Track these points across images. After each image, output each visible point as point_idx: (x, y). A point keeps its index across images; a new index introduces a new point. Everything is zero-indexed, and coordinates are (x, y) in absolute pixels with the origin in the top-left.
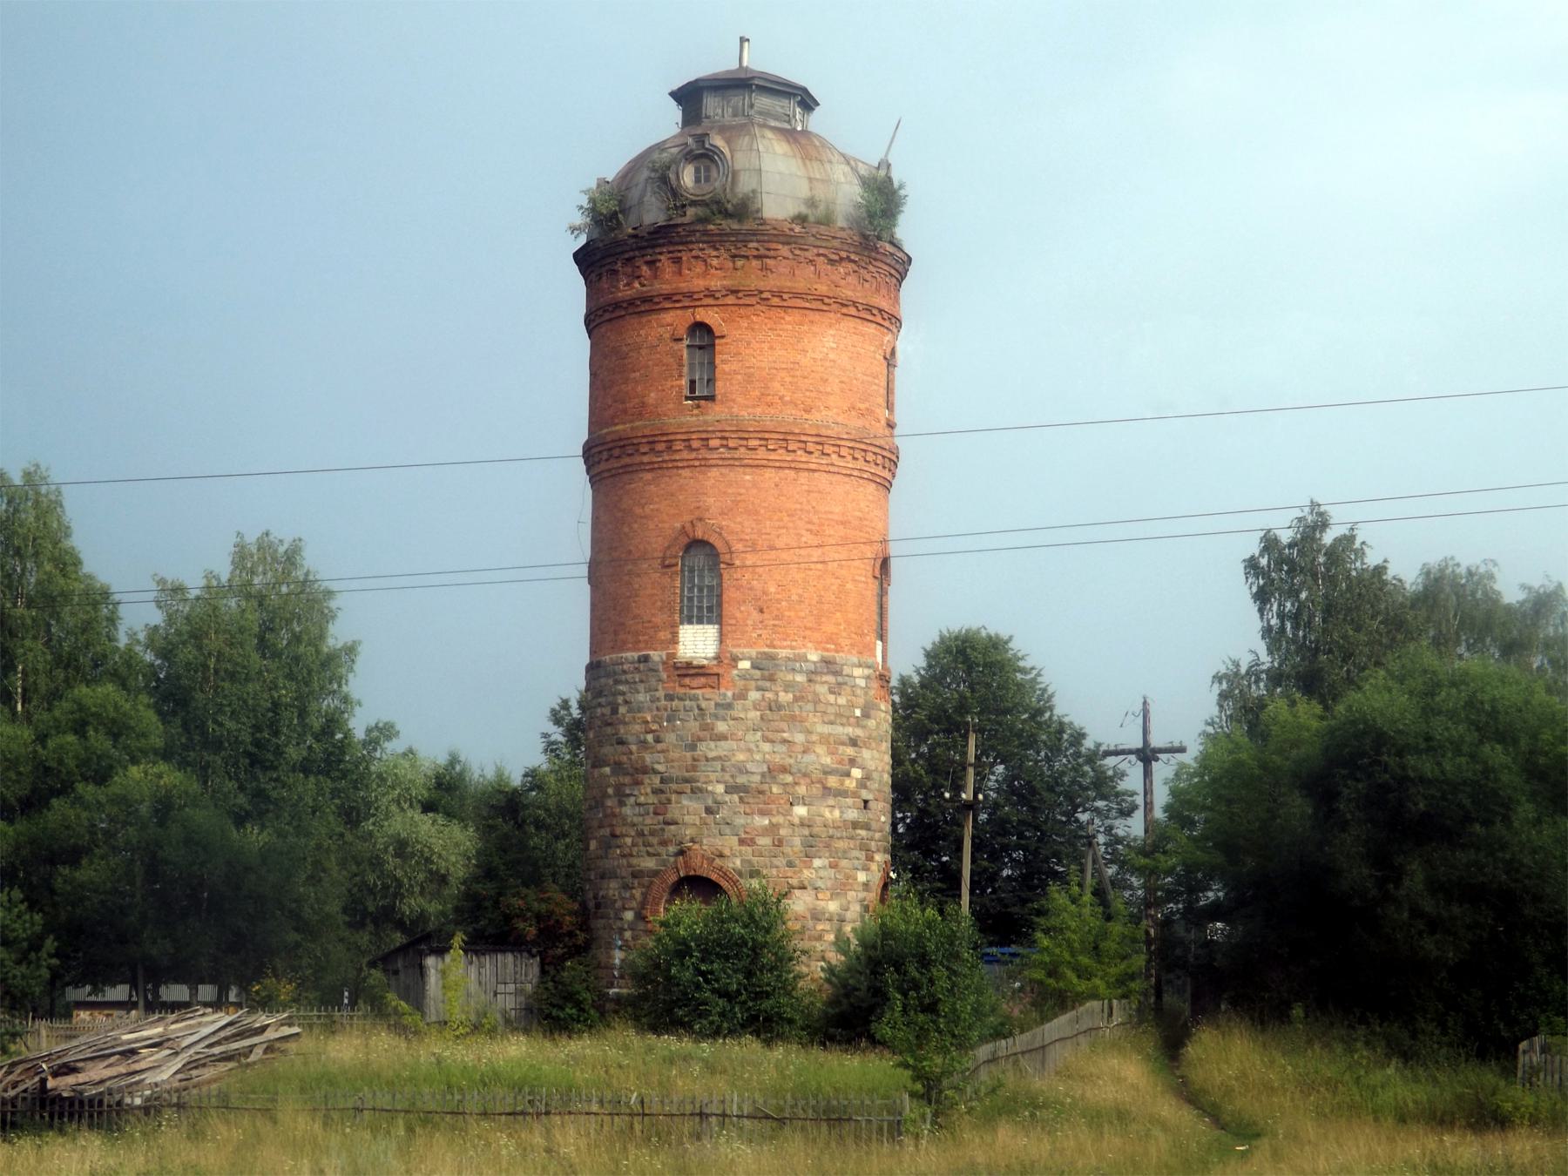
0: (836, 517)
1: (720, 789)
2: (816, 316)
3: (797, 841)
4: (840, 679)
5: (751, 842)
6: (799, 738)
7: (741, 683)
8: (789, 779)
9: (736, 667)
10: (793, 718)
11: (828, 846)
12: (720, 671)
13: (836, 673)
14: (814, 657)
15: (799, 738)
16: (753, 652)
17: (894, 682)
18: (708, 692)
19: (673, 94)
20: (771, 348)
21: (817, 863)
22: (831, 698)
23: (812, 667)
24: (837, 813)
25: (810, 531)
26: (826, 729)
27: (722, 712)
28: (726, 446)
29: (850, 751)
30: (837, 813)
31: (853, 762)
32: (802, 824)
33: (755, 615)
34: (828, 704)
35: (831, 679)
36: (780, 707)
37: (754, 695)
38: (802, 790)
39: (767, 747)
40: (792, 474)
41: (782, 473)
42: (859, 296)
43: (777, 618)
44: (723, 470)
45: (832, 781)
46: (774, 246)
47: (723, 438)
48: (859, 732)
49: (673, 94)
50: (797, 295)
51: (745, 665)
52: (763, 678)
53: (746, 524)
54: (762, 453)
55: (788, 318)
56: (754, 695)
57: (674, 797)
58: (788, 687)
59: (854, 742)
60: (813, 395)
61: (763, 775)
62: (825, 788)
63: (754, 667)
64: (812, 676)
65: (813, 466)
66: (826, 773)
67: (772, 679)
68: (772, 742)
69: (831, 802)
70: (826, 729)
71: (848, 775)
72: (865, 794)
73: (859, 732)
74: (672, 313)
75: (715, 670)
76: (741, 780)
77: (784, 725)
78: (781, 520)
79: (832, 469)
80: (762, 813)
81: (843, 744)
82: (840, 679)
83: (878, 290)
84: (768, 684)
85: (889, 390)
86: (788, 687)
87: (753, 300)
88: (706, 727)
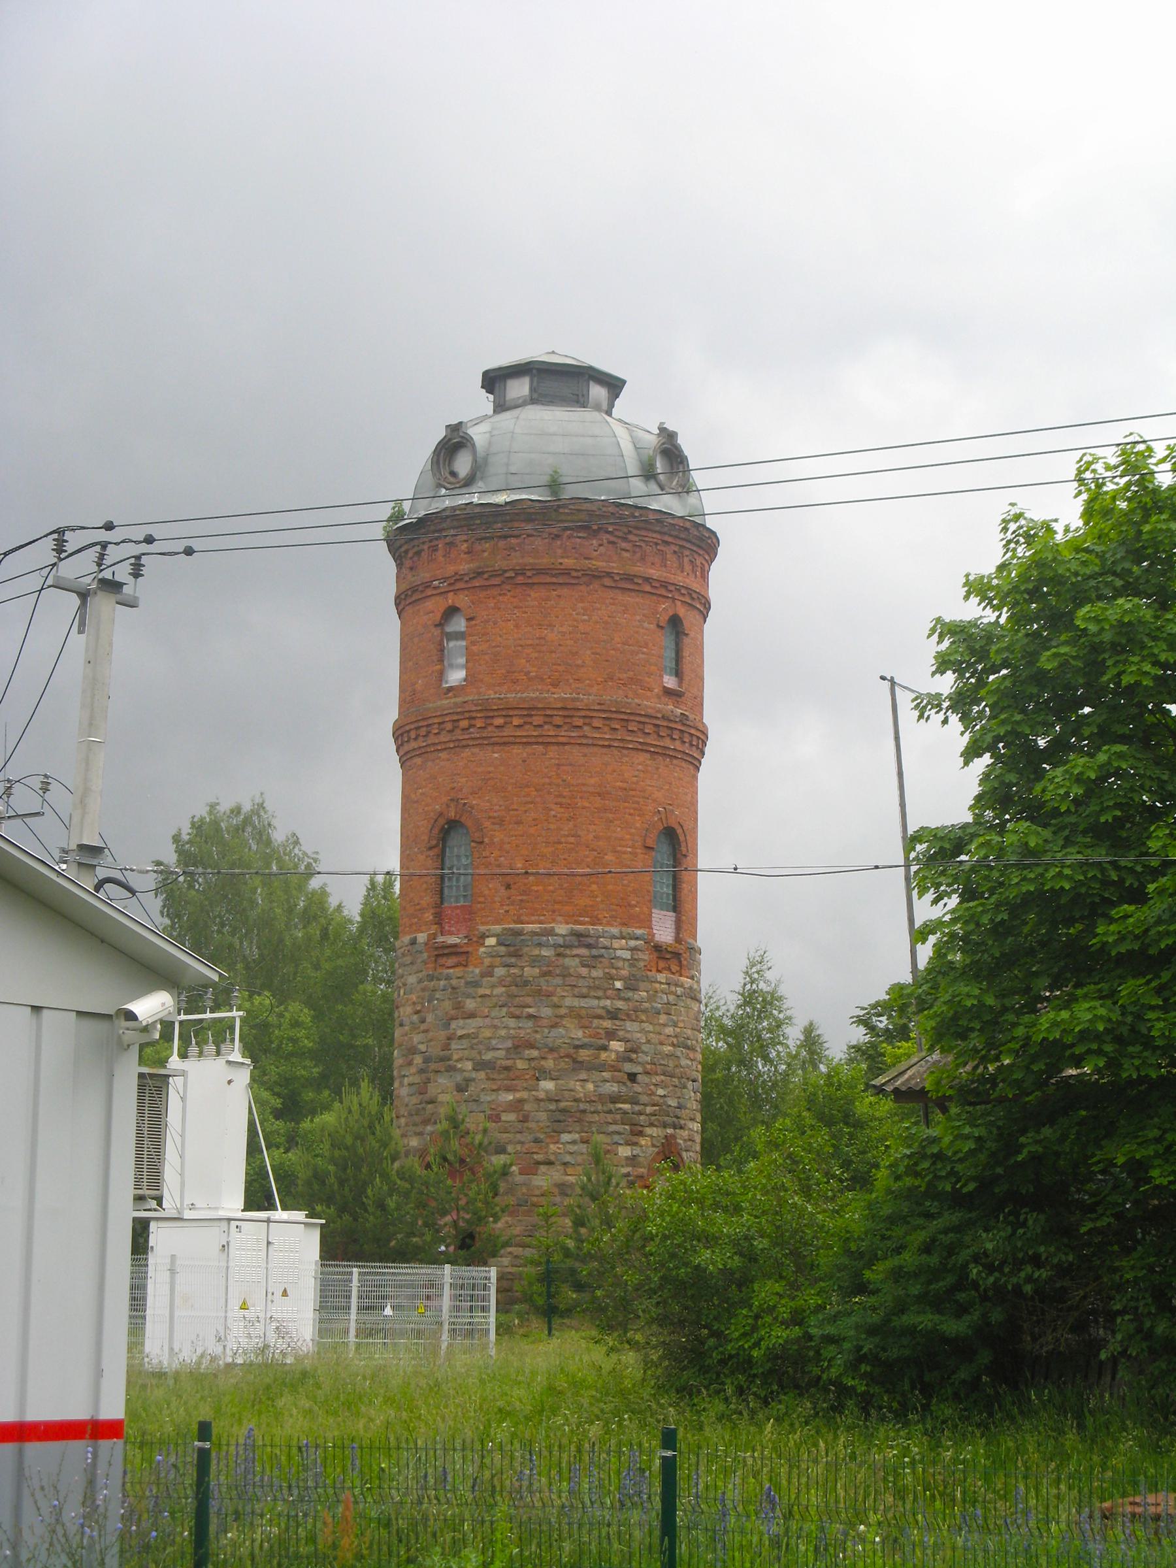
0: (591, 789)
1: (469, 1065)
2: (565, 591)
3: (543, 1116)
4: (595, 952)
5: (496, 1118)
6: (546, 1012)
7: (487, 961)
8: (535, 1053)
9: (483, 944)
10: (539, 992)
11: (579, 1121)
12: (470, 949)
13: (589, 946)
14: (562, 929)
15: (546, 1012)
16: (497, 928)
17: (144, 917)
18: (458, 971)
19: (624, 382)
20: (517, 626)
21: (565, 1137)
22: (584, 971)
23: (561, 941)
24: (590, 1086)
25: (561, 804)
26: (576, 1002)
27: (471, 990)
28: (642, 730)
29: (607, 1024)
30: (590, 1086)
31: (611, 1035)
32: (550, 1100)
33: (503, 891)
34: (580, 976)
35: (583, 951)
36: (526, 983)
37: (500, 972)
38: (549, 1064)
39: (512, 1023)
40: (540, 748)
41: (529, 749)
42: (615, 567)
43: (524, 893)
44: (476, 750)
45: (584, 1054)
46: (516, 524)
47: (470, 718)
48: (620, 1004)
49: (624, 382)
50: (540, 572)
51: (491, 941)
52: (510, 955)
53: (495, 800)
54: (507, 732)
55: (532, 594)
56: (500, 972)
57: (432, 1075)
58: (535, 961)
59: (613, 1015)
60: (561, 668)
61: (508, 1050)
62: (575, 1061)
63: (500, 944)
64: (561, 950)
65: (561, 740)
66: (577, 1047)
67: (517, 955)
68: (518, 1017)
69: (583, 1076)
70: (576, 1002)
71: (605, 1048)
72: (629, 1067)
73: (620, 1004)
74: (433, 600)
75: (465, 949)
76: (488, 1056)
77: (529, 1000)
78: (528, 795)
79: (584, 741)
80: (509, 1089)
81: (600, 1017)
82: (595, 952)
83: (643, 559)
84: (513, 960)
85: (678, 659)
86: (535, 961)
87: (497, 581)
88: (458, 1006)
